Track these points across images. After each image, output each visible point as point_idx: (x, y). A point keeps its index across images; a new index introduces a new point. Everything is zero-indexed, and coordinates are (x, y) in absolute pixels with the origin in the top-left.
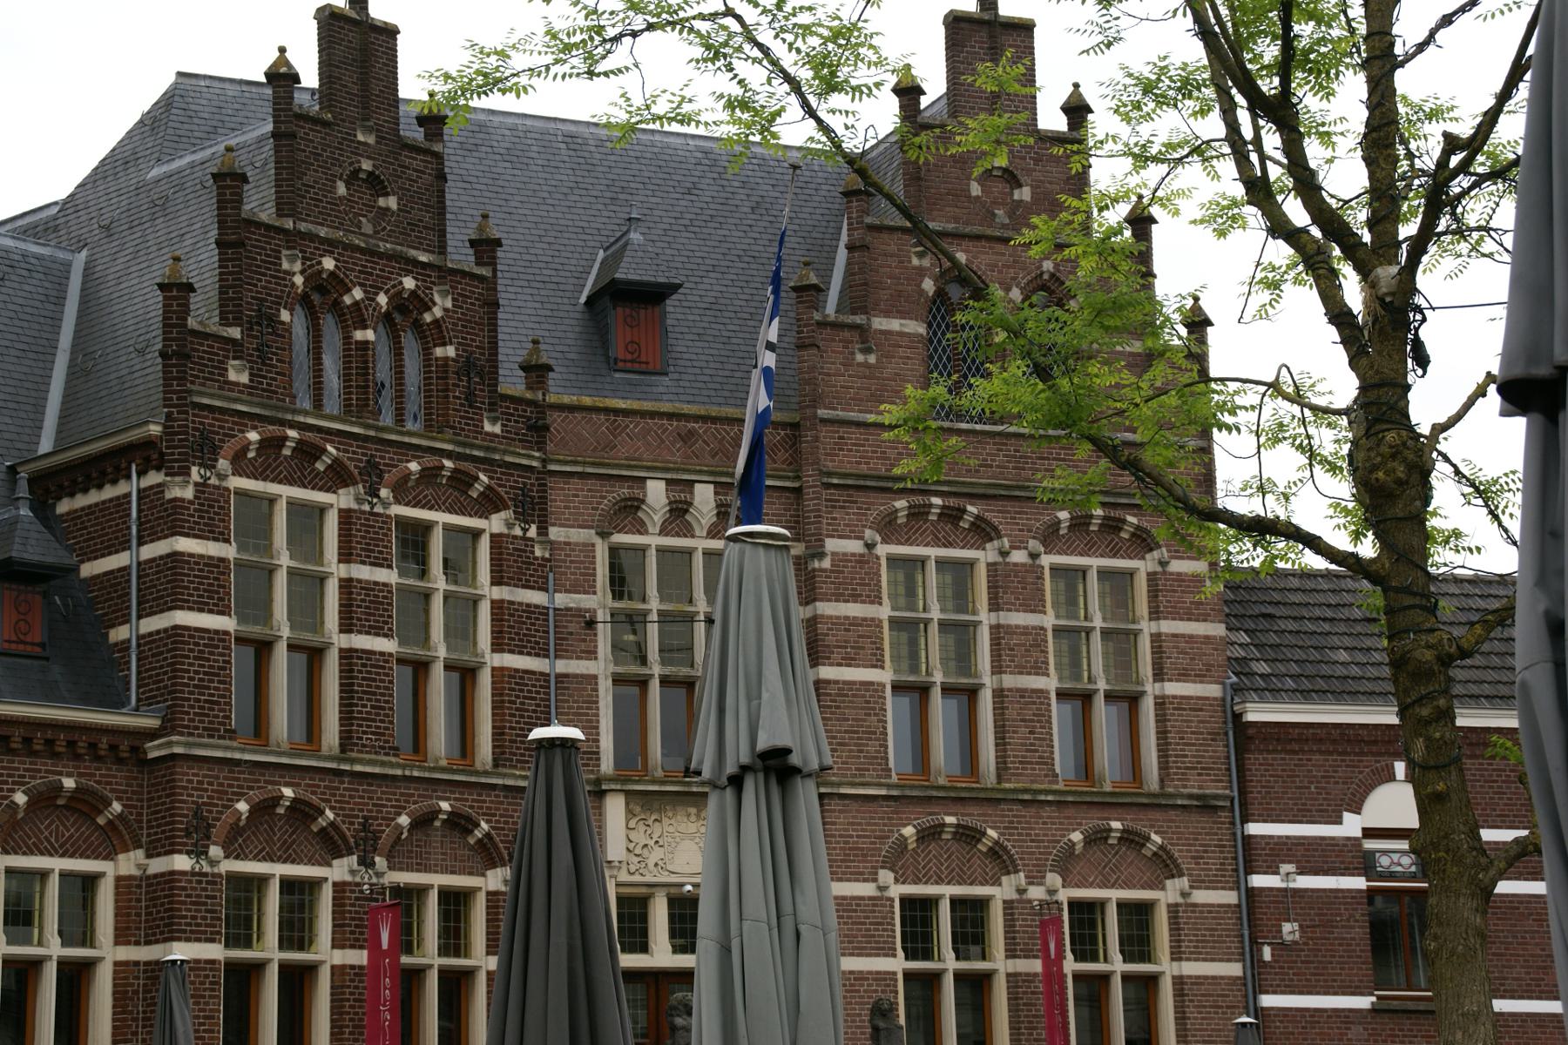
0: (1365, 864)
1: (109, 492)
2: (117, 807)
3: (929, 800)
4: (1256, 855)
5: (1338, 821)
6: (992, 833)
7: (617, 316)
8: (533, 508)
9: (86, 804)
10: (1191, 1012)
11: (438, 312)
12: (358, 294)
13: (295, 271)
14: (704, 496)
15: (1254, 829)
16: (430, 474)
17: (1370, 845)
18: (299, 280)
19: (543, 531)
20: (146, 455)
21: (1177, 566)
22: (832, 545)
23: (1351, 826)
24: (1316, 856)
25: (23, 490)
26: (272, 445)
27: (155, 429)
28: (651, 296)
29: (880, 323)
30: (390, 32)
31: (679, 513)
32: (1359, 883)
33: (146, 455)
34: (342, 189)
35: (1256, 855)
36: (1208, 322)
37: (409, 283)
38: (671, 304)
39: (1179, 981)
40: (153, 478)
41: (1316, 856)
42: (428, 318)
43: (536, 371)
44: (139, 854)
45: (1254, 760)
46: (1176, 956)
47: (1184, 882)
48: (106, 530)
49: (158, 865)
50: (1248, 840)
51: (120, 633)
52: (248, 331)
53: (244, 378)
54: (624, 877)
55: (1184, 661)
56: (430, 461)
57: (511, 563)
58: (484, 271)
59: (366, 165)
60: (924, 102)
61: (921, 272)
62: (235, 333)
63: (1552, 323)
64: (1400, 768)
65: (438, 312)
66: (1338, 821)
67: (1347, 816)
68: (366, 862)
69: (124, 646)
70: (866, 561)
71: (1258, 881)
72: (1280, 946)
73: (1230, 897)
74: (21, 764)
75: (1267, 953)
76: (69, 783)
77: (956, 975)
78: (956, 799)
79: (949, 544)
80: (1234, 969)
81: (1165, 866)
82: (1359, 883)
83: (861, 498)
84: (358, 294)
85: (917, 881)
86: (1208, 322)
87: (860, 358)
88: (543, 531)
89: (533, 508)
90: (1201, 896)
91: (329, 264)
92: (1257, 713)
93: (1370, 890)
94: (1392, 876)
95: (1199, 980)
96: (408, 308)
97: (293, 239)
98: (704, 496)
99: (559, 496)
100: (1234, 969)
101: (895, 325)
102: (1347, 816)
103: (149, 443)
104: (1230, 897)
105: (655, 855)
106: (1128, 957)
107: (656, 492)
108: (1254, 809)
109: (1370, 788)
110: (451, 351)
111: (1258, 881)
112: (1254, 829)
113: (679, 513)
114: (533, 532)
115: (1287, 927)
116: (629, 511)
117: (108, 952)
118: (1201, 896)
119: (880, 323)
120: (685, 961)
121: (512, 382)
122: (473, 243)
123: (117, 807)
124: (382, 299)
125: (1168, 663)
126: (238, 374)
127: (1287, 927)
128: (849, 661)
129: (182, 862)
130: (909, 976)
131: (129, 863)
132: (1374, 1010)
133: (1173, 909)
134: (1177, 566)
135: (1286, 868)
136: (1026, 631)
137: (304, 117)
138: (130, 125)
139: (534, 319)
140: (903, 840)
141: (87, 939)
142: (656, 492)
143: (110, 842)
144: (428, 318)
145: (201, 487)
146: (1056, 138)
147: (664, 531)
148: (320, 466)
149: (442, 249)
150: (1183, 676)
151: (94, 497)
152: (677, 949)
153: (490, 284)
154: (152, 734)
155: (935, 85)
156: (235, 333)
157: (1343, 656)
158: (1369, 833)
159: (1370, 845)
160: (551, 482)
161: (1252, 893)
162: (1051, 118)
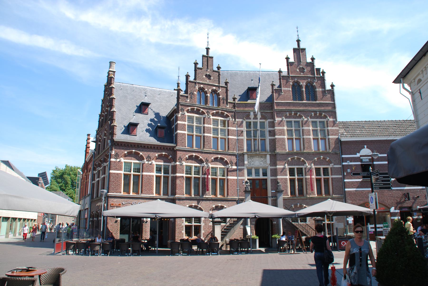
0: (361, 161)
3: (293, 154)
4: (344, 160)
5: (356, 154)
6: (302, 158)
10: (334, 183)
15: (343, 156)
17: (361, 158)
23: (358, 155)
24: (352, 160)
32: (360, 163)
35: (344, 160)
36: (325, 73)
39: (332, 178)
41: (352, 160)
43: (234, 99)
46: (332, 175)
47: (333, 164)
50: (342, 158)
54: (247, 166)
55: (332, 133)
64: (365, 146)
66: (356, 154)
67: (357, 154)
71: (344, 164)
72: (347, 173)
73: (340, 166)
75: (345, 174)
78: (297, 154)
80: (341, 176)
81: (329, 163)
82: (360, 163)
83: (282, 112)
85: (291, 165)
86: (325, 73)
90: (335, 166)
93: (361, 164)
94: (365, 162)
95: (335, 178)
100: (341, 176)
102: (357, 154)
104: (340, 166)
105: (252, 163)
106: (324, 175)
108: (343, 153)
109: (361, 149)
111: (344, 164)
112: (343, 156)
114: (234, 120)
115: (348, 170)
118: (335, 166)
120: (265, 177)
122: (194, 63)
125: (330, 133)
127: (348, 170)
128: (280, 135)
130: (124, 175)
132: (362, 181)
133: (331, 168)
135: (348, 161)
136: (307, 130)
138: (99, 111)
140: (289, 160)
147: (253, 119)
150: (332, 135)
153: (227, 88)
158: (361, 156)
159: (361, 158)
161: (343, 165)
162: (328, 87)
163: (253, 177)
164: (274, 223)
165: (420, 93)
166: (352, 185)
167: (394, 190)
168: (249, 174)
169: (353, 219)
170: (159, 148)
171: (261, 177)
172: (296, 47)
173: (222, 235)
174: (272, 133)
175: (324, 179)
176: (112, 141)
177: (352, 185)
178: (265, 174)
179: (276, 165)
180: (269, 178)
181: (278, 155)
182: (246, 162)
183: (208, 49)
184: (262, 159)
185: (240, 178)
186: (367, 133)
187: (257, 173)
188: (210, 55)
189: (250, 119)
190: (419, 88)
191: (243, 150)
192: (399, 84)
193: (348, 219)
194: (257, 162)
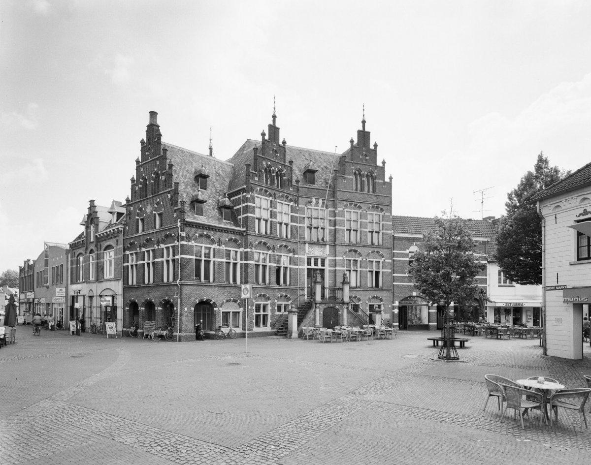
1: (238, 196)
2: (240, 242)
7: (307, 174)
8: (297, 202)
9: (235, 241)
11: (284, 172)
12: (273, 168)
13: (264, 163)
14: (321, 201)
16: (283, 196)
18: (265, 165)
19: (298, 205)
20: (244, 190)
21: (386, 214)
22: (338, 209)
25: (226, 196)
26: (261, 190)
27: (245, 186)
28: (314, 172)
29: (347, 176)
30: (279, 129)
31: (317, 203)
33: (244, 190)
34: (271, 152)
37: (280, 167)
38: (167, 138)
40: (245, 194)
42: (283, 172)
43: (297, 181)
44: (243, 249)
45: (395, 242)
46: (214, 257)
48: (237, 202)
49: (246, 250)
50: (393, 253)
51: (239, 217)
52: (258, 173)
53: (257, 179)
56: (283, 194)
57: (293, 210)
58: (291, 166)
59: (275, 149)
60: (354, 144)
61: (353, 169)
62: (256, 172)
63: (89, 274)
65: (284, 172)
68: (273, 251)
69: (240, 219)
70: (343, 211)
71: (394, 259)
73: (390, 261)
74: (227, 234)
76: (233, 238)
77: (204, 260)
78: (354, 246)
79: (355, 209)
84: (273, 168)
87: (344, 181)
88: (298, 205)
89: (297, 202)
91: (269, 163)
92: (396, 235)
96: (281, 170)
97: (264, 159)
98: (321, 201)
99: (301, 200)
100: (390, 271)
101: (348, 177)
103: (244, 189)
107: (314, 200)
110: (286, 178)
113: (317, 203)
116: (310, 202)
117: (239, 262)
119: (347, 176)
120: (323, 268)
121: (294, 183)
123: (240, 242)
124: (277, 169)
126: (256, 179)
128: (340, 226)
129: (249, 250)
130: (196, 260)
131: (242, 250)
134: (386, 214)
137: (266, 140)
139: (297, 174)
141: (379, 269)
142: (314, 200)
143: (239, 246)
144: (283, 172)
145: (251, 195)
146: (372, 150)
148: (268, 193)
149: (285, 162)
150: (386, 230)
151: (236, 197)
152: (322, 266)
153: (291, 168)
154: (244, 231)
155: (356, 141)
156: (256, 172)
157: (407, 228)
158: (410, 252)
160: (300, 198)
163: (313, 266)
164: (339, 313)
165: (556, 217)
166: (401, 279)
167: (383, 284)
168: (309, 264)
169: (398, 311)
170: (220, 231)
171: (320, 267)
172: (361, 129)
173: (298, 321)
174: (335, 224)
175: (241, 264)
176: (183, 220)
177: (401, 279)
178: (323, 264)
179: (335, 256)
180: (327, 268)
181: (338, 246)
182: (307, 251)
183: (364, 122)
184: (322, 249)
185: (300, 267)
186: (411, 228)
187: (316, 264)
188: (367, 130)
189: (318, 206)
190: (556, 213)
191: (304, 238)
192: (336, 153)
193: (394, 311)
194: (317, 252)
